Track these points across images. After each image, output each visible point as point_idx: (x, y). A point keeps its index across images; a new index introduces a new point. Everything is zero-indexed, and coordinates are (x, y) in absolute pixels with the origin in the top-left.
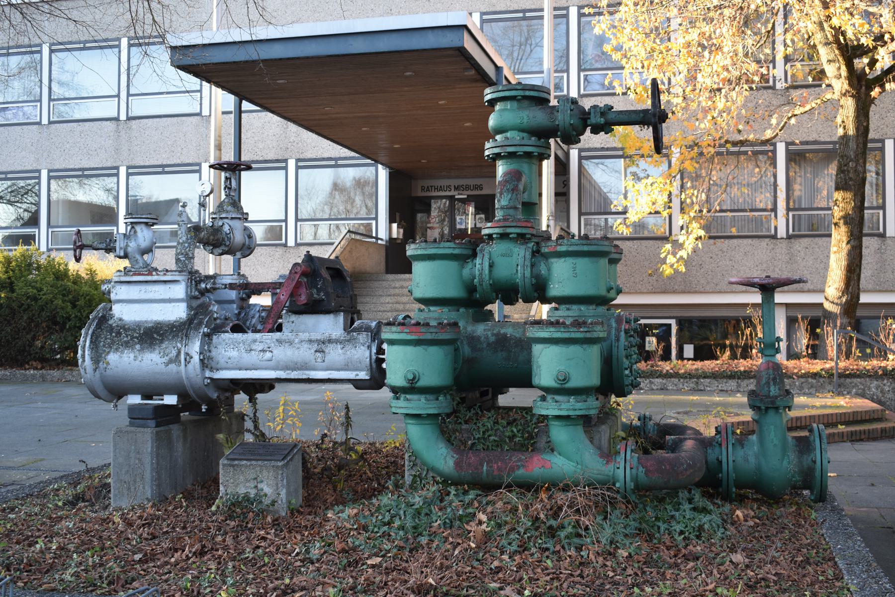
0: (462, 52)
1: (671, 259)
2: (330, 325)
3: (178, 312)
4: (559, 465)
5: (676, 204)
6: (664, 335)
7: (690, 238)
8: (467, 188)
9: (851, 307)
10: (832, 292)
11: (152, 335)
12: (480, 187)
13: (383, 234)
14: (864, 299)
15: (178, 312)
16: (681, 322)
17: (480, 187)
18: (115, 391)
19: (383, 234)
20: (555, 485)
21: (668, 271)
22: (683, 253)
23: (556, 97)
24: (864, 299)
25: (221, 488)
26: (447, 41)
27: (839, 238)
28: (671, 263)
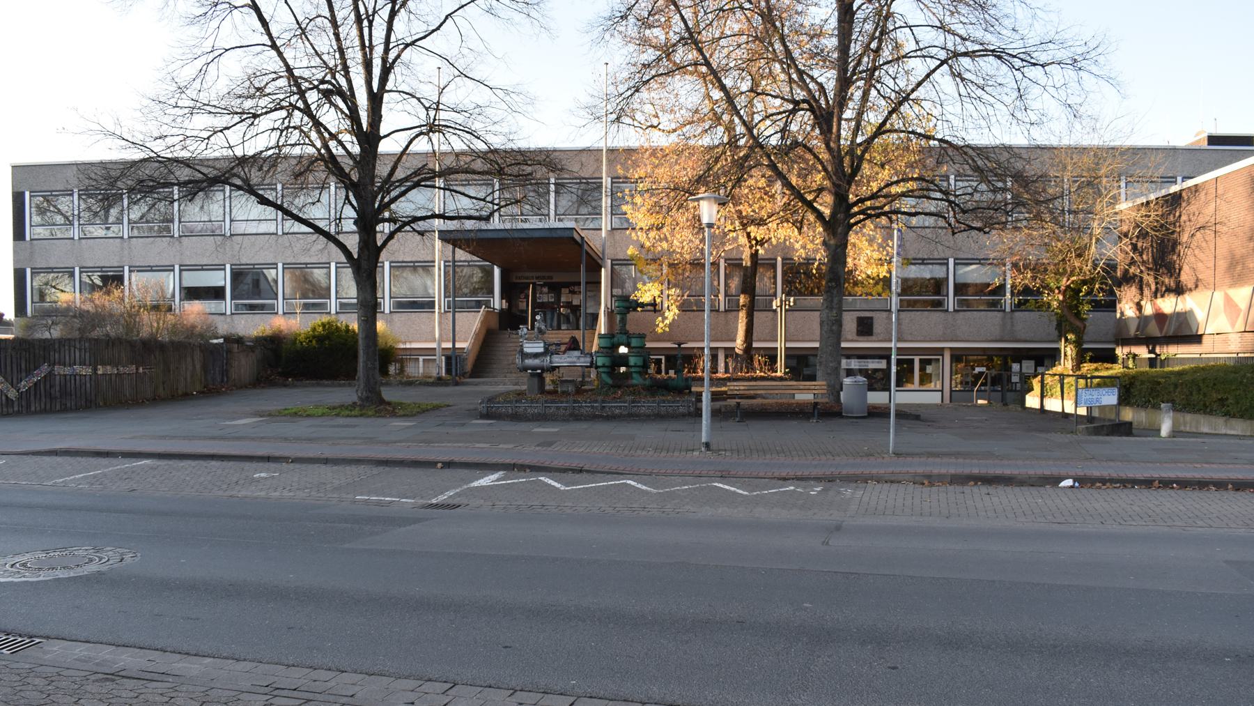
0: (573, 239)
1: (661, 325)
2: (577, 353)
3: (542, 350)
4: (635, 382)
5: (665, 297)
6: (658, 362)
7: (671, 314)
8: (544, 278)
9: (748, 349)
10: (739, 344)
11: (536, 355)
12: (551, 278)
13: (497, 306)
14: (755, 345)
15: (542, 350)
16: (668, 358)
17: (551, 278)
18: (525, 369)
19: (497, 306)
20: (633, 386)
21: (660, 331)
22: (667, 322)
23: (667, 373)
24: (755, 345)
25: (849, 260)
26: (567, 234)
27: (742, 315)
28: (661, 326)
